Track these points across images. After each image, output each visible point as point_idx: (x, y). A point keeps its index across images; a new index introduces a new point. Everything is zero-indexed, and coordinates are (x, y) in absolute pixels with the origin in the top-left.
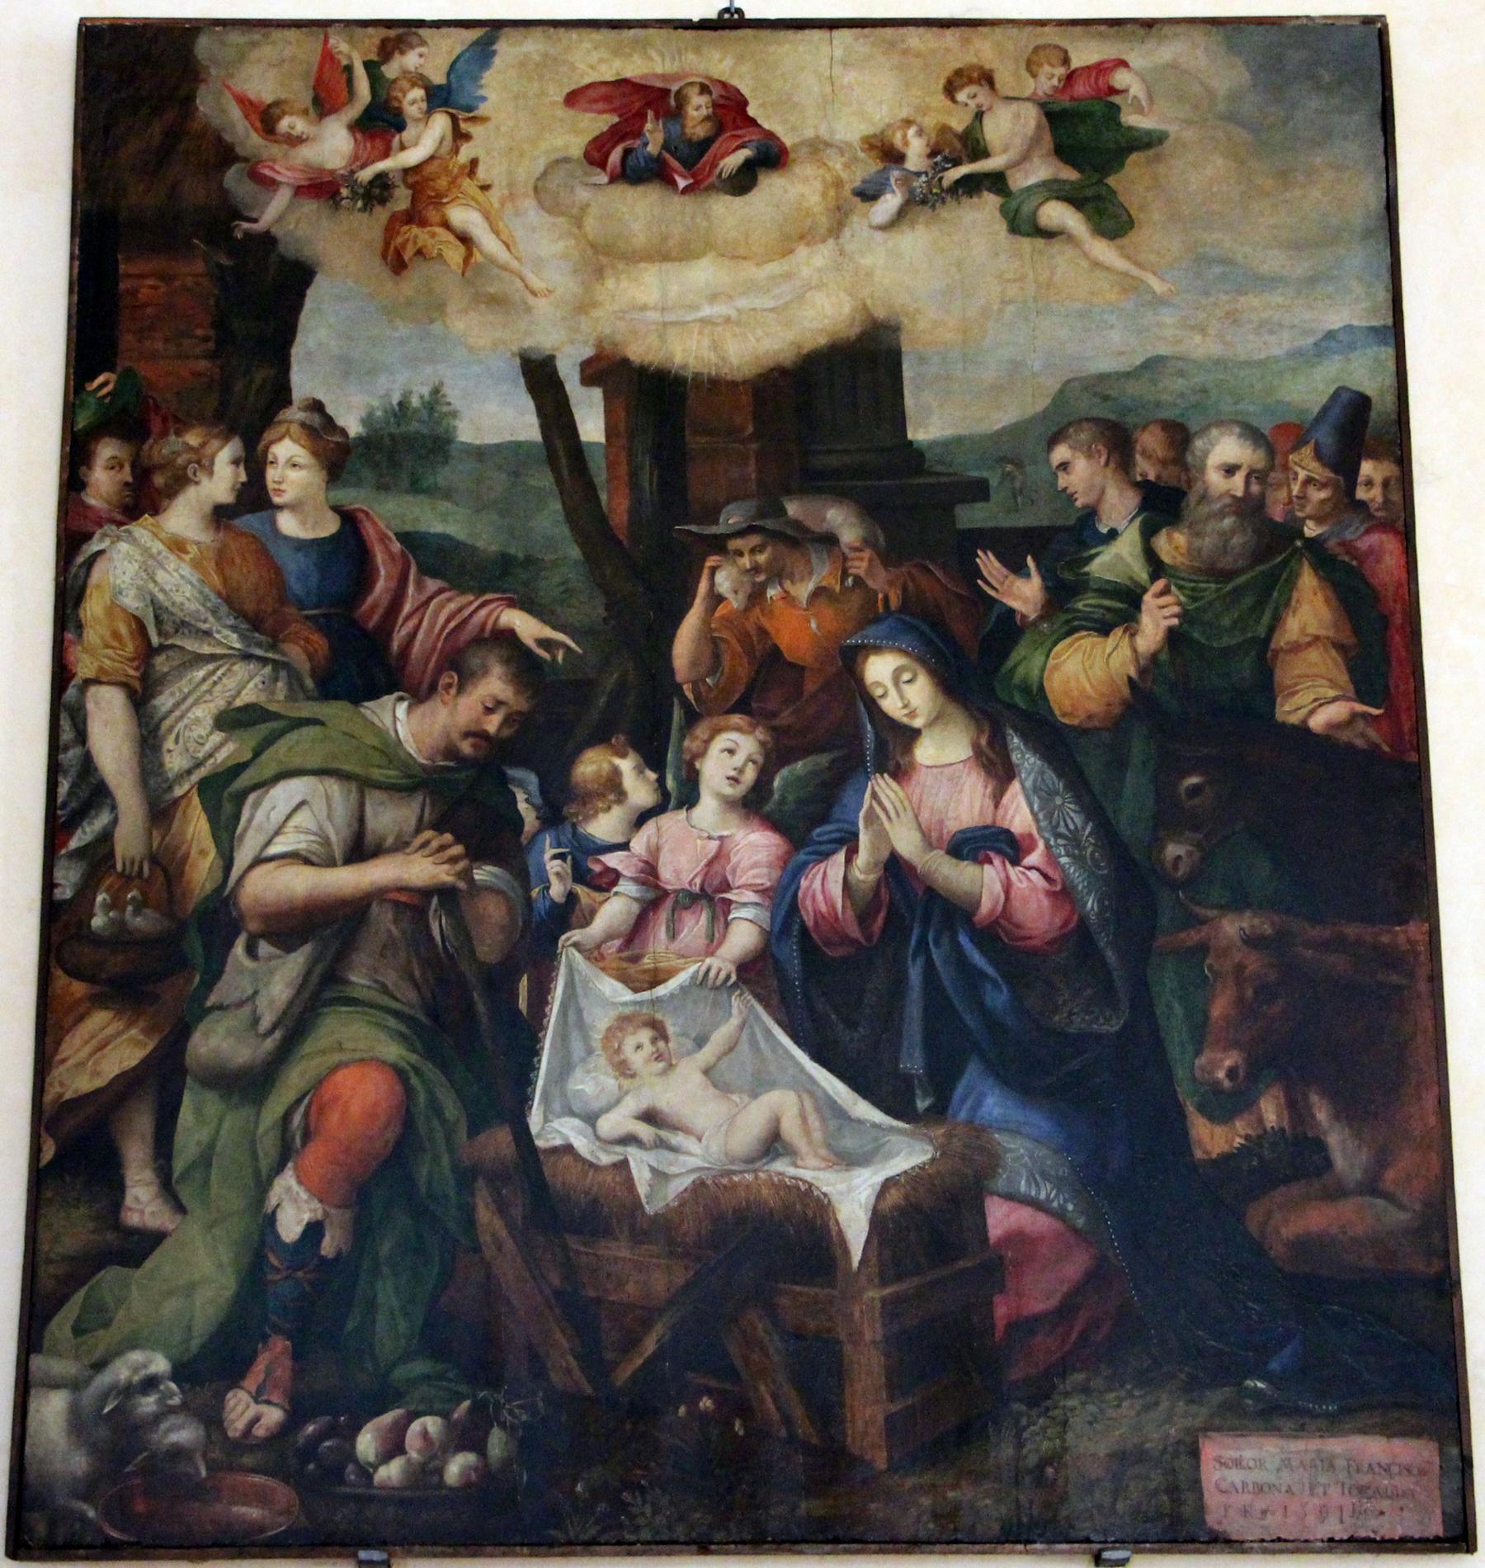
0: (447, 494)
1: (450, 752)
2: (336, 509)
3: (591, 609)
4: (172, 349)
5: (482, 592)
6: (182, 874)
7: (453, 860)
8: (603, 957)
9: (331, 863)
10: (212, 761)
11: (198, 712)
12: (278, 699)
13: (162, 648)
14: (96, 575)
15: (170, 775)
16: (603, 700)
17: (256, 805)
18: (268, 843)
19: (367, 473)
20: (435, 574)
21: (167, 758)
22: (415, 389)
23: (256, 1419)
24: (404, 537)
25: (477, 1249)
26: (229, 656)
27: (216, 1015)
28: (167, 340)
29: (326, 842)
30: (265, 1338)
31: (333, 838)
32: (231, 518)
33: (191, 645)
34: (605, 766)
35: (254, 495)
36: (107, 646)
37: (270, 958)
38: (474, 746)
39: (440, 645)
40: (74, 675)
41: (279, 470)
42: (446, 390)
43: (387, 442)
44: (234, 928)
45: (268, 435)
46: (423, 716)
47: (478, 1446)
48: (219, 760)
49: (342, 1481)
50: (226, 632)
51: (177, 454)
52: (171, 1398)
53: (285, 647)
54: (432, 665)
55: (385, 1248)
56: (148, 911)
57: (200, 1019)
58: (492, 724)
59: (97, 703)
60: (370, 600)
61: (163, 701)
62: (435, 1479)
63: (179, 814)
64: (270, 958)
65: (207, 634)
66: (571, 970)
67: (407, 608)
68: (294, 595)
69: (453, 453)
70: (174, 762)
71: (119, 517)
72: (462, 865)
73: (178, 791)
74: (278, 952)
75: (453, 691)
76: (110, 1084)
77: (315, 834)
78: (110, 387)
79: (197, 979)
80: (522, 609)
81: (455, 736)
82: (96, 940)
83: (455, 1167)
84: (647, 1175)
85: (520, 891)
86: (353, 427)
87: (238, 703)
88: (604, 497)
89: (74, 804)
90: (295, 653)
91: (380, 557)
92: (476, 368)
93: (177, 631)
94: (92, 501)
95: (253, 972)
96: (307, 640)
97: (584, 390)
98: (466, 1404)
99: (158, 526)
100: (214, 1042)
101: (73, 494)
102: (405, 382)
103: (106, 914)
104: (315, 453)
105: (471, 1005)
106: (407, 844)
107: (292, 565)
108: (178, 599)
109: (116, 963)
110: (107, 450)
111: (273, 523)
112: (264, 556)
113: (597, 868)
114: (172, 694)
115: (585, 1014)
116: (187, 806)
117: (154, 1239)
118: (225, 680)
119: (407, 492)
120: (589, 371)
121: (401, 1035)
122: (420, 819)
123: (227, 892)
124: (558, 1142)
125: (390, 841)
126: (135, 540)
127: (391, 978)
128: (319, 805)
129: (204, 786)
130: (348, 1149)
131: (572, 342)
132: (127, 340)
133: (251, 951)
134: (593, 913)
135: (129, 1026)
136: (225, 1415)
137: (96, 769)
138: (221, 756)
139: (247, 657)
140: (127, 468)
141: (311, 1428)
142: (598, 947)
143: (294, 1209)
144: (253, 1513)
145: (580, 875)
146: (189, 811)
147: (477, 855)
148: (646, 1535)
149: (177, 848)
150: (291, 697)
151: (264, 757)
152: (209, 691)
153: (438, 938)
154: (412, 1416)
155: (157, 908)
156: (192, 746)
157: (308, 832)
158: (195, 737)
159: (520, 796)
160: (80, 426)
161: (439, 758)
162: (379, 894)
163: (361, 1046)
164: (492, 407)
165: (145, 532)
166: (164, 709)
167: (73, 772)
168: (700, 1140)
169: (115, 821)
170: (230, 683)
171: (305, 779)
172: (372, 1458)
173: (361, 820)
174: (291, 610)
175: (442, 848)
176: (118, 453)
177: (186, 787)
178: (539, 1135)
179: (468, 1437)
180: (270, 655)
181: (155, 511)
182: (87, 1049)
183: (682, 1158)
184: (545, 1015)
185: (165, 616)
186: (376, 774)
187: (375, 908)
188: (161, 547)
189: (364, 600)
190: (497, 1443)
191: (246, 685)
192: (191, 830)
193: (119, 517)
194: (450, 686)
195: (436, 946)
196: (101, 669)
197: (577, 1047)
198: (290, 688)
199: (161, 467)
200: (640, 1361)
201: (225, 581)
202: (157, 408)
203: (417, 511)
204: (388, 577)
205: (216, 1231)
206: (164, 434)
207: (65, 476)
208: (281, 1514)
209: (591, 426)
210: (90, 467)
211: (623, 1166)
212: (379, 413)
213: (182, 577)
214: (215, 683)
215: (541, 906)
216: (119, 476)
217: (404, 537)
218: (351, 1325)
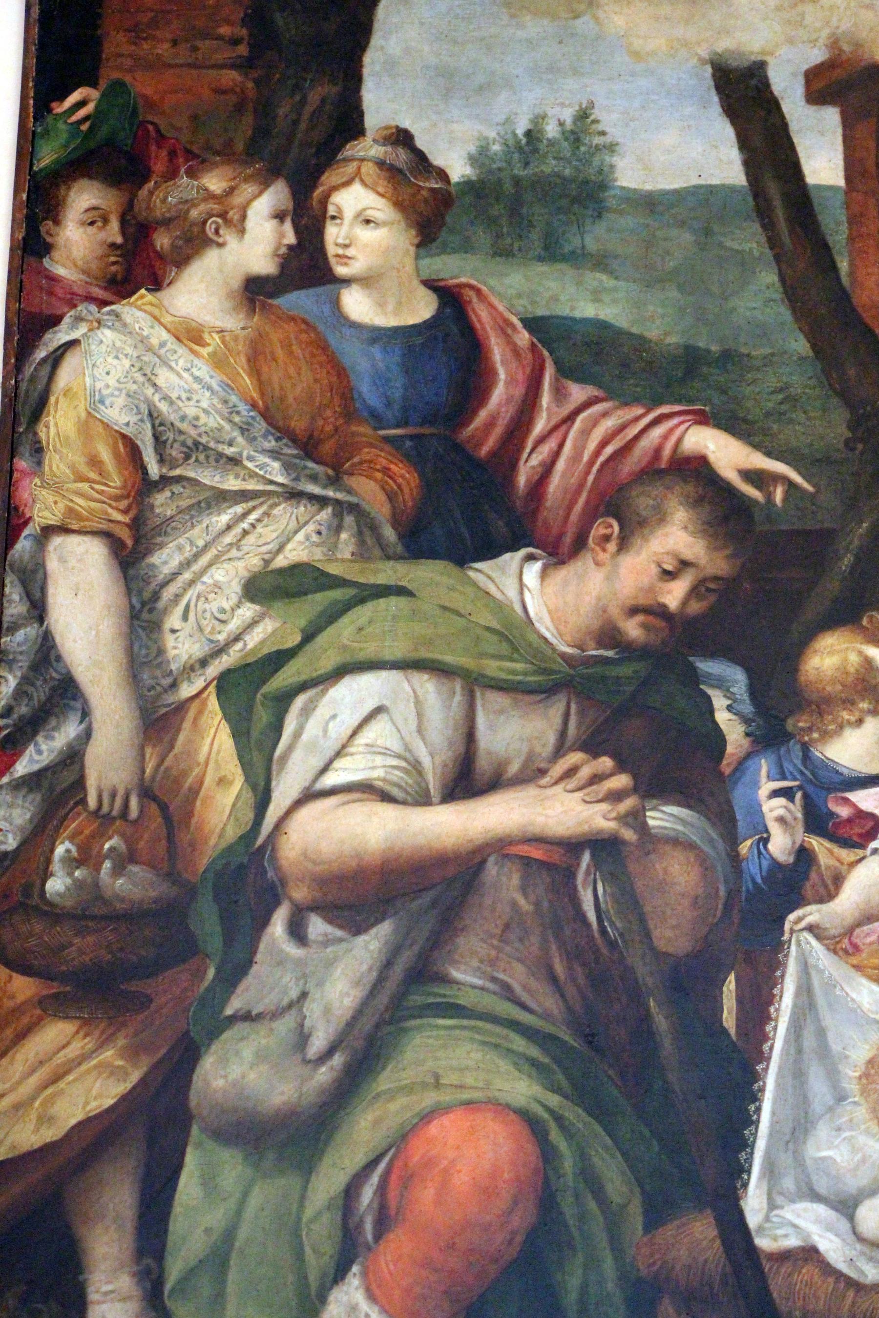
0: (601, 262)
1: (608, 635)
2: (430, 284)
3: (831, 426)
4: (183, 54)
5: (658, 401)
6: (190, 814)
7: (615, 797)
8: (856, 948)
9: (423, 800)
10: (239, 646)
11: (218, 574)
12: (342, 557)
13: (165, 481)
15: (174, 667)
16: (847, 560)
17: (307, 712)
18: (325, 770)
19: (482, 237)
20: (582, 379)
21: (170, 641)
22: (550, 112)
24: (532, 324)
26: (269, 494)
27: (241, 1028)
28: (175, 43)
29: (416, 767)
31: (426, 761)
32: (272, 295)
33: (209, 477)
34: (853, 658)
35: (308, 263)
37: (327, 942)
38: (644, 626)
39: (591, 478)
42: (596, 114)
43: (508, 187)
44: (271, 896)
45: (329, 178)
46: (566, 583)
48: (250, 645)
50: (263, 459)
51: (191, 203)
56: (134, 869)
57: (213, 1034)
58: (673, 595)
59: (62, 560)
60: (483, 415)
61: (165, 559)
63: (187, 725)
64: (327, 942)
65: (234, 461)
66: (805, 968)
67: (540, 426)
69: (612, 203)
70: (181, 645)
72: (629, 803)
73: (186, 691)
74: (339, 933)
75: (612, 547)
76: (68, 1136)
77: (399, 757)
78: (90, 108)
79: (211, 973)
80: (718, 426)
81: (615, 612)
82: (53, 913)
83: (623, 1277)
85: (721, 845)
86: (458, 169)
87: (281, 562)
88: (843, 265)
89: (23, 710)
91: (497, 352)
92: (643, 82)
93: (187, 457)
94: (61, 271)
95: (300, 963)
96: (386, 471)
97: (812, 110)
99: (160, 306)
100: (235, 1071)
101: (32, 260)
102: (535, 102)
103: (70, 874)
104: (398, 205)
105: (646, 1018)
106: (543, 772)
107: (364, 365)
108: (191, 411)
109: (83, 949)
110: (84, 197)
111: (336, 303)
112: (321, 347)
113: (844, 812)
114: (180, 548)
115: (831, 1036)
116: (200, 712)
118: (259, 529)
119: (540, 259)
120: (819, 85)
121: (534, 1063)
122: (563, 734)
123: (260, 841)
124: (793, 1242)
125: (514, 768)
126: (125, 325)
127: (517, 976)
128: (404, 712)
129: (224, 683)
130: (452, 1246)
131: (791, 41)
132: (116, 43)
133: (297, 931)
134: (838, 880)
135: (100, 1046)
137: (59, 658)
138: (253, 639)
139: (294, 495)
140: (115, 224)
142: (850, 931)
145: (817, 821)
146: (204, 718)
147: (654, 786)
149: (184, 774)
150: (362, 555)
151: (322, 639)
152: (237, 544)
153: (592, 916)
155: (151, 865)
156: (208, 624)
157: (386, 752)
158: (213, 606)
159: (719, 702)
160: (43, 164)
161: (592, 644)
162: (500, 847)
163: (470, 1081)
164: (669, 138)
165: (139, 314)
166: (166, 570)
167: (24, 662)
169: (88, 734)
170: (269, 533)
171: (384, 674)
173: (470, 736)
175: (596, 779)
177: (200, 683)
178: (760, 1229)
180: (330, 493)
181: (156, 284)
182: (33, 1081)
184: (765, 1038)
186: (493, 668)
187: (492, 868)
188: (165, 335)
189: (475, 412)
191: (295, 536)
192: (205, 749)
194: (607, 538)
195: (588, 925)
196: (71, 512)
197: (818, 1087)
198: (361, 542)
199: (166, 223)
201: (262, 385)
203: (553, 285)
204: (511, 381)
206: (172, 174)
207: (20, 236)
209: (823, 161)
210: (57, 222)
212: (496, 148)
213: (197, 379)
214: (245, 533)
215: (754, 869)
216: (102, 235)
217: (532, 324)
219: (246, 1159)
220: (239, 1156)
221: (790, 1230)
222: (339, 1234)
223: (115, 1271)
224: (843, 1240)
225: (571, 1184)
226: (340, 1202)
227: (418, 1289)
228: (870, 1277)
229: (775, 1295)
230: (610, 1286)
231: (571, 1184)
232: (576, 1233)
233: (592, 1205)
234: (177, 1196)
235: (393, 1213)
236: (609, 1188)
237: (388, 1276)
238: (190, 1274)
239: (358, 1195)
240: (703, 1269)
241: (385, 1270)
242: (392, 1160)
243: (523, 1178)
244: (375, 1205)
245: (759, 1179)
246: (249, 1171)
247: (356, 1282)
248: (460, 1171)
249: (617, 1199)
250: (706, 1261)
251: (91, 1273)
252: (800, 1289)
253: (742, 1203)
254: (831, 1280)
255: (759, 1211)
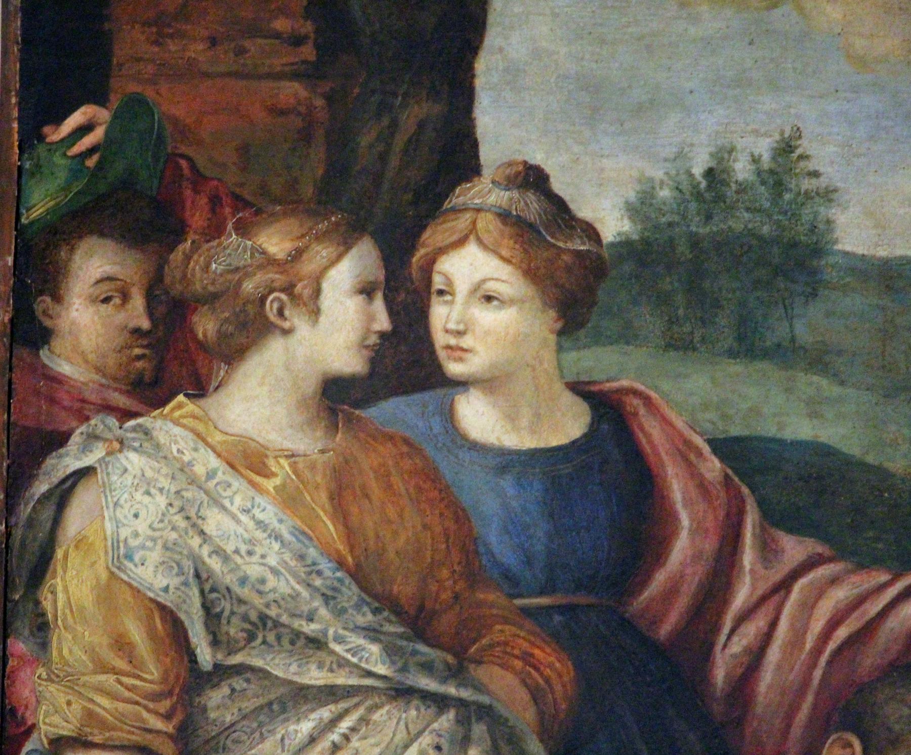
0: (819, 360)
2: (579, 389)
13: (221, 672)
14: (75, 520)
19: (648, 320)
20: (797, 525)
22: (740, 144)
28: (213, 42)
33: (282, 667)
35: (406, 360)
36: (103, 668)
39: (818, 674)
40: (30, 731)
41: (458, 307)
42: (805, 145)
50: (357, 640)
51: (243, 272)
53: (481, 673)
54: (803, 715)
60: (660, 579)
65: (317, 643)
67: (741, 597)
68: (497, 564)
69: (831, 275)
71: (121, 400)
86: (612, 220)
90: (502, 686)
91: (677, 488)
93: (251, 637)
94: (65, 368)
96: (527, 658)
99: (205, 419)
101: (22, 352)
104: (530, 274)
107: (492, 505)
108: (254, 570)
111: (449, 415)
119: (732, 354)
139: (401, 693)
140: (138, 302)
160: (36, 214)
174: (492, 597)
176: (109, 269)
180: (452, 690)
181: (200, 388)
185: (226, 605)
188: (214, 462)
189: (644, 583)
193: (121, 400)
199: (211, 299)
201: (350, 533)
202: (199, 179)
204: (698, 529)
206: (215, 231)
210: (58, 298)
212: (665, 193)
213: (260, 524)
216: (120, 318)
217: (727, 448)
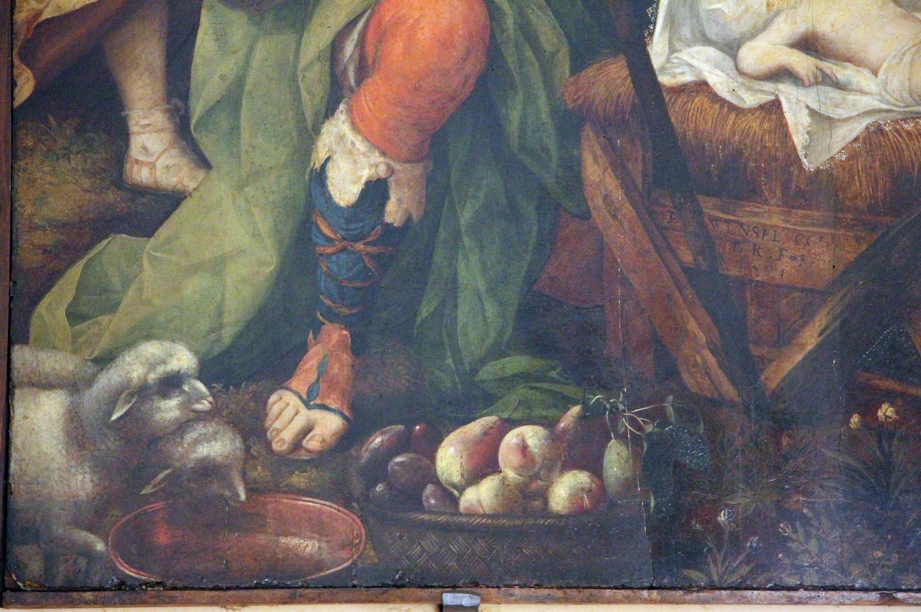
23: (307, 430)
25: (586, 216)
30: (317, 328)
47: (595, 467)
49: (420, 508)
52: (198, 401)
55: (466, 216)
62: (537, 504)
83: (553, 112)
84: (805, 119)
98: (576, 410)
117: (169, 201)
124: (688, 78)
130: (417, 89)
136: (268, 423)
141: (378, 440)
143: (349, 164)
144: (307, 546)
148: (812, 578)
154: (508, 424)
168: (875, 72)
172: (456, 478)
178: (663, 68)
179: (581, 452)
183: (851, 97)
190: (616, 460)
200: (799, 358)
205: (250, 191)
208: (343, 547)
211: (774, 107)
218: (425, 311)
219: (250, 18)
220: (245, 18)
221: (687, 69)
222: (328, 79)
223: (150, 109)
224: (728, 74)
225: (512, 37)
226: (328, 55)
227: (391, 123)
228: (748, 102)
229: (673, 120)
230: (544, 117)
231: (512, 37)
232: (517, 78)
233: (529, 54)
234: (196, 49)
235: (370, 62)
236: (543, 39)
237: (367, 112)
238: (210, 111)
239: (342, 48)
240: (617, 101)
241: (366, 108)
242: (368, 20)
243: (474, 33)
244: (356, 57)
245: (663, 28)
246: (254, 30)
247: (343, 117)
248: (422, 28)
249: (548, 48)
250: (619, 95)
251: (130, 110)
252: (693, 115)
253: (648, 48)
254: (717, 106)
255: (661, 55)
